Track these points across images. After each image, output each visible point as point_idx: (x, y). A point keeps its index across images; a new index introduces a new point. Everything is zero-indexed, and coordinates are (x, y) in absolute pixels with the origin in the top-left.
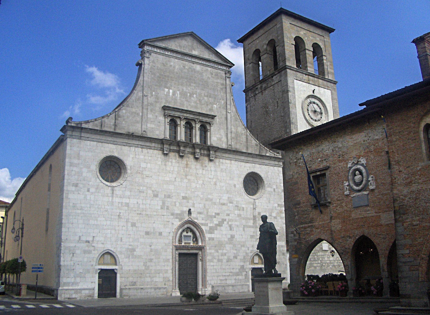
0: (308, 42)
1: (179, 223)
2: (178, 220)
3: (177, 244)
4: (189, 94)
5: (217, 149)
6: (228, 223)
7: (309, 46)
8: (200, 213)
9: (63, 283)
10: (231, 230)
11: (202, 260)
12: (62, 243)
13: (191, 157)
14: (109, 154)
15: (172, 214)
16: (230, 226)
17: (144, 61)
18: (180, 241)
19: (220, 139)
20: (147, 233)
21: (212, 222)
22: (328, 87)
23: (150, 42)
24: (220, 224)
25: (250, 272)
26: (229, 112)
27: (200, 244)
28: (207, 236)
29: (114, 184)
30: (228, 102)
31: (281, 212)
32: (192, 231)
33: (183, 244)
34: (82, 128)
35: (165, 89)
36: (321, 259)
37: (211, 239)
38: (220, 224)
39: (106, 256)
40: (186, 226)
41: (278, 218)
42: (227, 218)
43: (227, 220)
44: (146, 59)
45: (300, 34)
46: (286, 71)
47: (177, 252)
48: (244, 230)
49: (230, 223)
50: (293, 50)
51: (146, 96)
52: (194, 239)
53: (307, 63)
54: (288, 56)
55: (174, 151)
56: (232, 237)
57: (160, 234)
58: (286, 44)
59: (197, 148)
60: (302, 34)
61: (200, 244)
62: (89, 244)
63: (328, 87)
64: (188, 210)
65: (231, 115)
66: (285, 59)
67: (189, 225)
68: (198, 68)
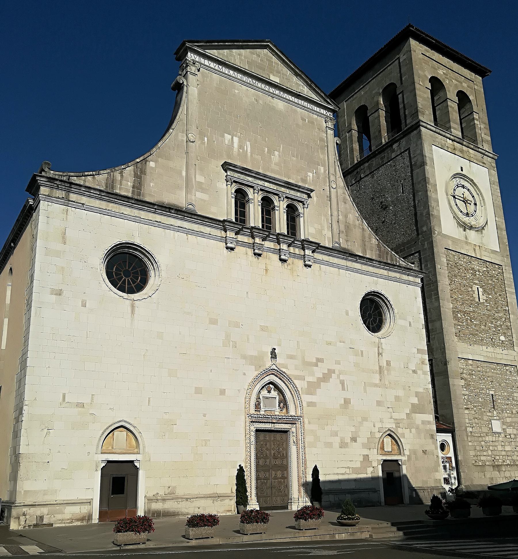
0: (451, 89)
1: (256, 373)
2: (253, 367)
3: (252, 411)
4: (266, 149)
5: (317, 247)
6: (338, 377)
7: (452, 95)
8: (291, 357)
9: (23, 492)
10: (343, 389)
11: (297, 443)
12: (25, 407)
13: (275, 257)
14: (124, 239)
15: (244, 357)
16: (342, 383)
17: (186, 79)
18: (258, 406)
19: (320, 232)
20: (198, 391)
21: (312, 374)
22: (484, 163)
23: (198, 46)
24: (326, 378)
25: (380, 467)
26: (334, 186)
27: (292, 412)
28: (306, 398)
29: (135, 296)
30: (332, 171)
31: (423, 363)
32: (277, 387)
33: (262, 413)
34: (71, 183)
35: (226, 135)
36: (491, 448)
37: (311, 404)
38: (326, 378)
39: (116, 432)
40: (267, 379)
41: (419, 372)
42: (337, 368)
43: (337, 372)
44: (190, 77)
45: (438, 73)
46: (420, 131)
47: (253, 429)
48: (365, 391)
49: (342, 377)
50: (428, 98)
51: (193, 142)
52: (282, 405)
53: (449, 121)
54: (421, 107)
55: (244, 244)
56: (347, 402)
57: (223, 392)
58: (417, 86)
59: (284, 242)
60: (440, 73)
61: (292, 412)
62: (83, 409)
63: (484, 163)
64: (271, 350)
65: (337, 192)
66: (417, 112)
67: (273, 378)
68: (280, 105)
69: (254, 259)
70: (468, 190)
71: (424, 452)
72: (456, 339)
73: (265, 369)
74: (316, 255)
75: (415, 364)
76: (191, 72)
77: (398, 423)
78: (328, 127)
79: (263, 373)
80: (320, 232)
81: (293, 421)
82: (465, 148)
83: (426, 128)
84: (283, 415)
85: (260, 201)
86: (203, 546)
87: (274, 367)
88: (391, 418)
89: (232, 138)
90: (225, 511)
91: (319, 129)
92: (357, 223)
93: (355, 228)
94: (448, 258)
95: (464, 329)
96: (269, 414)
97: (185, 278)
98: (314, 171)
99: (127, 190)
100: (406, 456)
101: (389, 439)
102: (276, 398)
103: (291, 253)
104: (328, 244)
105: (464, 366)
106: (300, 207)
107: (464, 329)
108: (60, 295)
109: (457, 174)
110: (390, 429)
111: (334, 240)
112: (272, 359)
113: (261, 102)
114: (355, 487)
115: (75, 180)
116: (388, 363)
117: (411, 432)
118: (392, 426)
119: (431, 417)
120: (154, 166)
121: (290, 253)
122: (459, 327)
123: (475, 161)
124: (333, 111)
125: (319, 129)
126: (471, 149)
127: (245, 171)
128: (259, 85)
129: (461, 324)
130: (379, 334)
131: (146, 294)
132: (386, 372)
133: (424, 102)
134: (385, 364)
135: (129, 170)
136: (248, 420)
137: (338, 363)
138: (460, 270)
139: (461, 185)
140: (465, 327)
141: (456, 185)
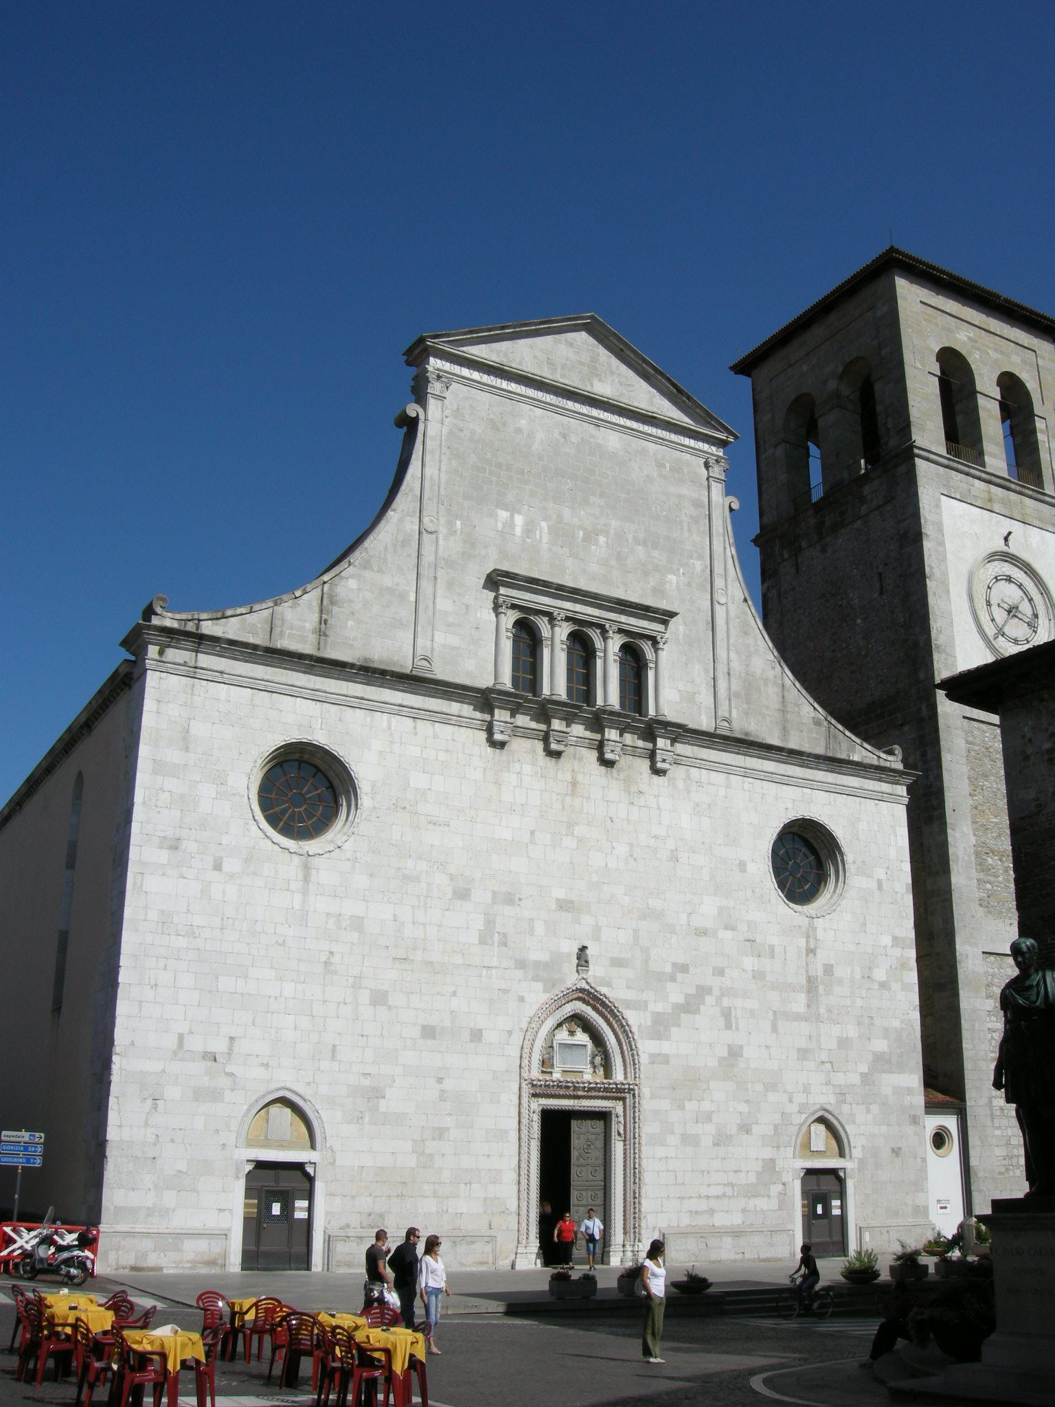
2: (540, 985)
3: (536, 1073)
5: (680, 732)
8: (618, 963)
10: (728, 1026)
15: (521, 964)
16: (727, 1014)
18: (547, 1064)
20: (429, 1032)
24: (690, 1006)
26: (723, 601)
28: (646, 1047)
29: (312, 846)
32: (588, 1027)
33: (557, 1076)
38: (690, 1006)
40: (569, 1009)
41: (895, 986)
42: (715, 982)
43: (716, 992)
48: (774, 1029)
49: (726, 1002)
55: (526, 734)
56: (734, 1053)
57: (477, 1035)
61: (618, 1076)
67: (579, 1007)
68: (612, 441)
69: (550, 763)
70: (1020, 586)
71: (896, 1152)
72: (980, 912)
73: (563, 989)
74: (680, 748)
75: (887, 970)
76: (434, 395)
77: (841, 1095)
78: (713, 477)
79: (559, 996)
80: (690, 698)
81: (620, 1093)
82: (1013, 496)
83: (927, 459)
84: (598, 1081)
85: (945, 453)
86: (426, 1389)
87: (584, 985)
88: (828, 1083)
89: (512, 517)
90: (474, 1263)
91: (694, 482)
92: (771, 674)
93: (766, 685)
94: (971, 739)
95: (999, 889)
96: (569, 1080)
97: (408, 807)
98: (681, 570)
99: (303, 639)
100: (856, 1160)
101: (822, 1128)
102: (585, 1046)
103: (627, 746)
104: (704, 722)
105: (996, 970)
106: (647, 648)
107: (999, 889)
108: (176, 848)
109: (994, 554)
110: (825, 1106)
111: (720, 713)
112: (579, 968)
113: (573, 439)
114: (744, 1222)
115: (208, 628)
116: (828, 970)
117: (868, 1111)
118: (823, 1098)
119: (914, 1079)
120: (355, 587)
121: (624, 745)
122: (989, 886)
123: (1036, 522)
124: (722, 444)
125: (694, 482)
126: (1026, 496)
127: (533, 584)
128: (570, 404)
129: (992, 879)
130: (810, 909)
131: (332, 841)
132: (821, 989)
133: (1000, 356)
134: (820, 972)
135: (311, 598)
136: (526, 1090)
137: (720, 972)
138: (995, 762)
139: (1005, 576)
140: (1002, 885)
141: (993, 577)
